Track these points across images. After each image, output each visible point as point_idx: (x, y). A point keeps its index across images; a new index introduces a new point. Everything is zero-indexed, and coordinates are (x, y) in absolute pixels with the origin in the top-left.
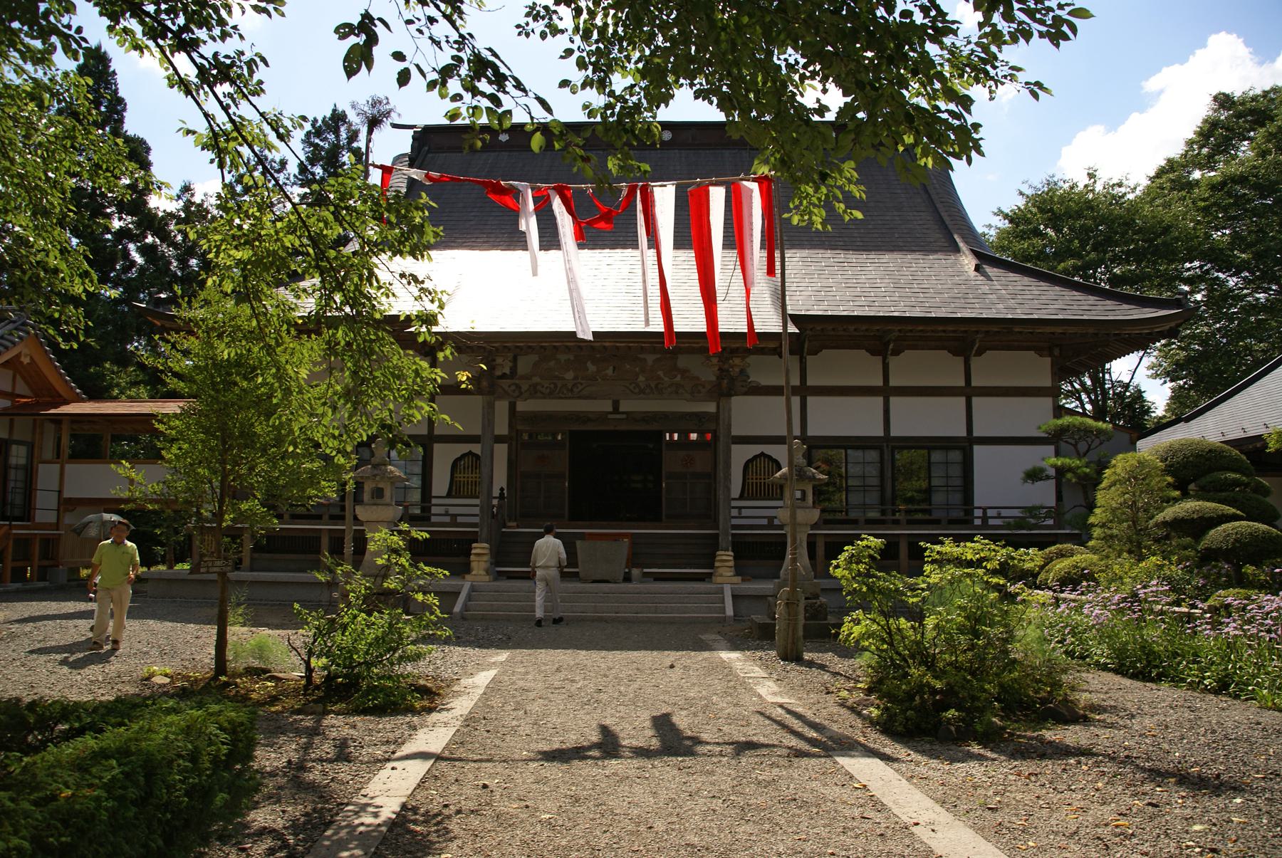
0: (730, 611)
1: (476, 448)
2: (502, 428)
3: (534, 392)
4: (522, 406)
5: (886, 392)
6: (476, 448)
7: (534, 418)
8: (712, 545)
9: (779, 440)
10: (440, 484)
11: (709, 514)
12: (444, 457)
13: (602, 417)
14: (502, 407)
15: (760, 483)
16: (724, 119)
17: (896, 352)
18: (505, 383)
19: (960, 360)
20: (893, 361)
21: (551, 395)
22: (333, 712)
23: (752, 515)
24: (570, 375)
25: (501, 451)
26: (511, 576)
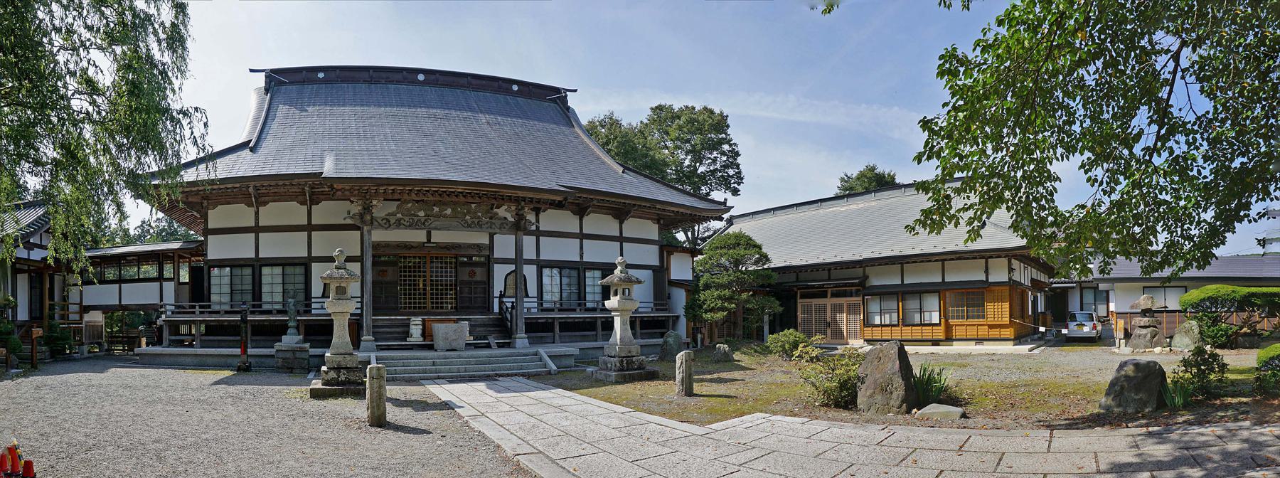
26: (389, 348)
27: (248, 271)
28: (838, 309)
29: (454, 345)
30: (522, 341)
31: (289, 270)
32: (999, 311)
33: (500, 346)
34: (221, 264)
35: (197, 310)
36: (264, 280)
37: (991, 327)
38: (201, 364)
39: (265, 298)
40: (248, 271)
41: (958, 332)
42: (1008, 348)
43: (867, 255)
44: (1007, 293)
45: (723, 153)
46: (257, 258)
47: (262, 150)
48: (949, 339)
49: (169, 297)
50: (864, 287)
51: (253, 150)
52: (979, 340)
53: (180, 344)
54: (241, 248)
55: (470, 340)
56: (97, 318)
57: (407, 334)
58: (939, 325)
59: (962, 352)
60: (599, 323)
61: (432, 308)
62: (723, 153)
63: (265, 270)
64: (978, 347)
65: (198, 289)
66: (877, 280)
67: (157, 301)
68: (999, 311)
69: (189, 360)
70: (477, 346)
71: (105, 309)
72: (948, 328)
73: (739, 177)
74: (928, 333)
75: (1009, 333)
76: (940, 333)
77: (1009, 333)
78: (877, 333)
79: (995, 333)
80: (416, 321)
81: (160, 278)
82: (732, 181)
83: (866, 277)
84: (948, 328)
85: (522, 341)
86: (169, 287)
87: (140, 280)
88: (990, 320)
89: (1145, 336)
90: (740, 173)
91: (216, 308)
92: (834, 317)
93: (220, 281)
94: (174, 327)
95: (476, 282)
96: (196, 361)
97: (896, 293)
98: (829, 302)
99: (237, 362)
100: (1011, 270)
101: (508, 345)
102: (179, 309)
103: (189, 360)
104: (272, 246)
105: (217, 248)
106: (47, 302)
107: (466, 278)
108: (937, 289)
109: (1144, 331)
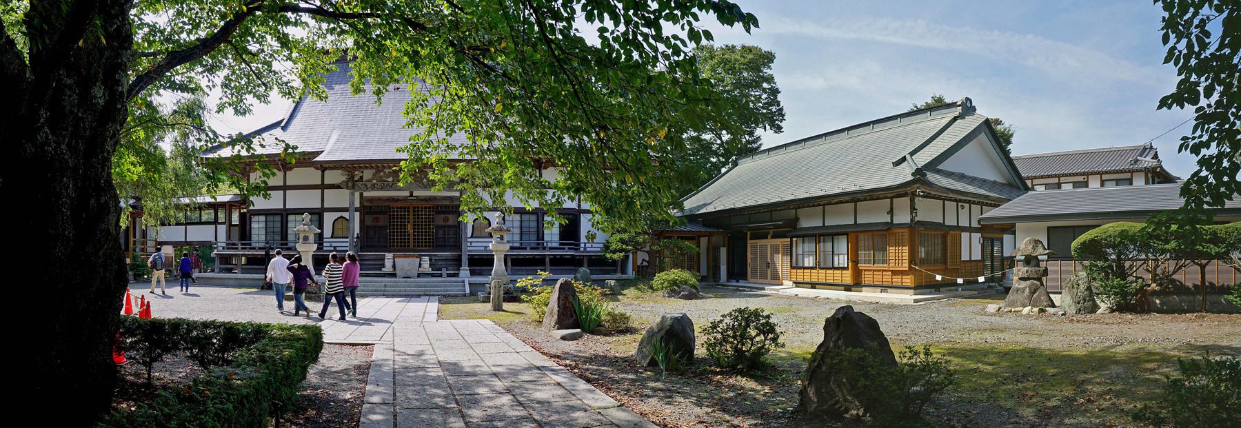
0: (468, 291)
1: (346, 215)
2: (357, 204)
3: (374, 187)
4: (365, 194)
5: (323, 187)
6: (346, 215)
7: (372, 199)
8: (458, 262)
9: (345, 210)
10: (328, 232)
11: (457, 245)
12: (329, 218)
13: (405, 199)
14: (357, 195)
15: (482, 230)
16: (599, 46)
17: (546, 168)
18: (359, 184)
19: (319, 172)
20: (544, 171)
21: (382, 189)
22: (1117, 362)
23: (473, 246)
24: (390, 179)
25: (357, 215)
26: (367, 275)
27: (278, 218)
28: (775, 250)
29: (409, 274)
30: (465, 272)
31: (270, 218)
32: (899, 256)
33: (449, 275)
34: (259, 213)
35: (240, 246)
36: (290, 225)
37: (894, 273)
38: (240, 284)
39: (546, 238)
40: (278, 218)
41: (867, 278)
42: (908, 297)
43: (802, 195)
44: (906, 236)
45: (764, 90)
46: (285, 209)
47: (291, 128)
48: (857, 284)
49: (222, 237)
50: (795, 229)
51: (284, 129)
52: (885, 288)
53: (230, 271)
54: (275, 201)
55: (429, 271)
56: (168, 251)
57: (383, 266)
58: (847, 268)
59: (896, 302)
60: (547, 259)
61: (402, 247)
62: (764, 90)
63: (291, 218)
64: (884, 295)
65: (244, 231)
66: (809, 221)
67: (213, 239)
68: (899, 256)
69: (231, 282)
70: (433, 275)
71: (175, 244)
72: (857, 274)
73: (781, 113)
74: (838, 276)
75: (908, 280)
76: (847, 277)
77: (908, 280)
78: (807, 276)
79: (897, 280)
80: (389, 256)
81: (215, 222)
82: (774, 120)
83: (797, 219)
84: (857, 274)
85: (465, 272)
86: (222, 229)
87: (201, 223)
88: (893, 267)
89: (1024, 290)
90: (781, 109)
91: (254, 245)
92: (772, 257)
93: (258, 226)
94: (226, 260)
95: (449, 226)
96: (237, 282)
97: (815, 236)
98: (769, 242)
99: (261, 283)
100: (913, 209)
101: (456, 275)
102: (231, 245)
103: (231, 282)
104: (296, 200)
105: (259, 202)
106: (132, 239)
107: (441, 223)
108: (852, 233)
109: (1023, 284)
